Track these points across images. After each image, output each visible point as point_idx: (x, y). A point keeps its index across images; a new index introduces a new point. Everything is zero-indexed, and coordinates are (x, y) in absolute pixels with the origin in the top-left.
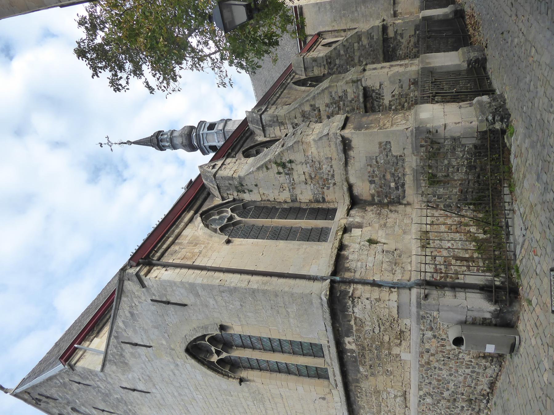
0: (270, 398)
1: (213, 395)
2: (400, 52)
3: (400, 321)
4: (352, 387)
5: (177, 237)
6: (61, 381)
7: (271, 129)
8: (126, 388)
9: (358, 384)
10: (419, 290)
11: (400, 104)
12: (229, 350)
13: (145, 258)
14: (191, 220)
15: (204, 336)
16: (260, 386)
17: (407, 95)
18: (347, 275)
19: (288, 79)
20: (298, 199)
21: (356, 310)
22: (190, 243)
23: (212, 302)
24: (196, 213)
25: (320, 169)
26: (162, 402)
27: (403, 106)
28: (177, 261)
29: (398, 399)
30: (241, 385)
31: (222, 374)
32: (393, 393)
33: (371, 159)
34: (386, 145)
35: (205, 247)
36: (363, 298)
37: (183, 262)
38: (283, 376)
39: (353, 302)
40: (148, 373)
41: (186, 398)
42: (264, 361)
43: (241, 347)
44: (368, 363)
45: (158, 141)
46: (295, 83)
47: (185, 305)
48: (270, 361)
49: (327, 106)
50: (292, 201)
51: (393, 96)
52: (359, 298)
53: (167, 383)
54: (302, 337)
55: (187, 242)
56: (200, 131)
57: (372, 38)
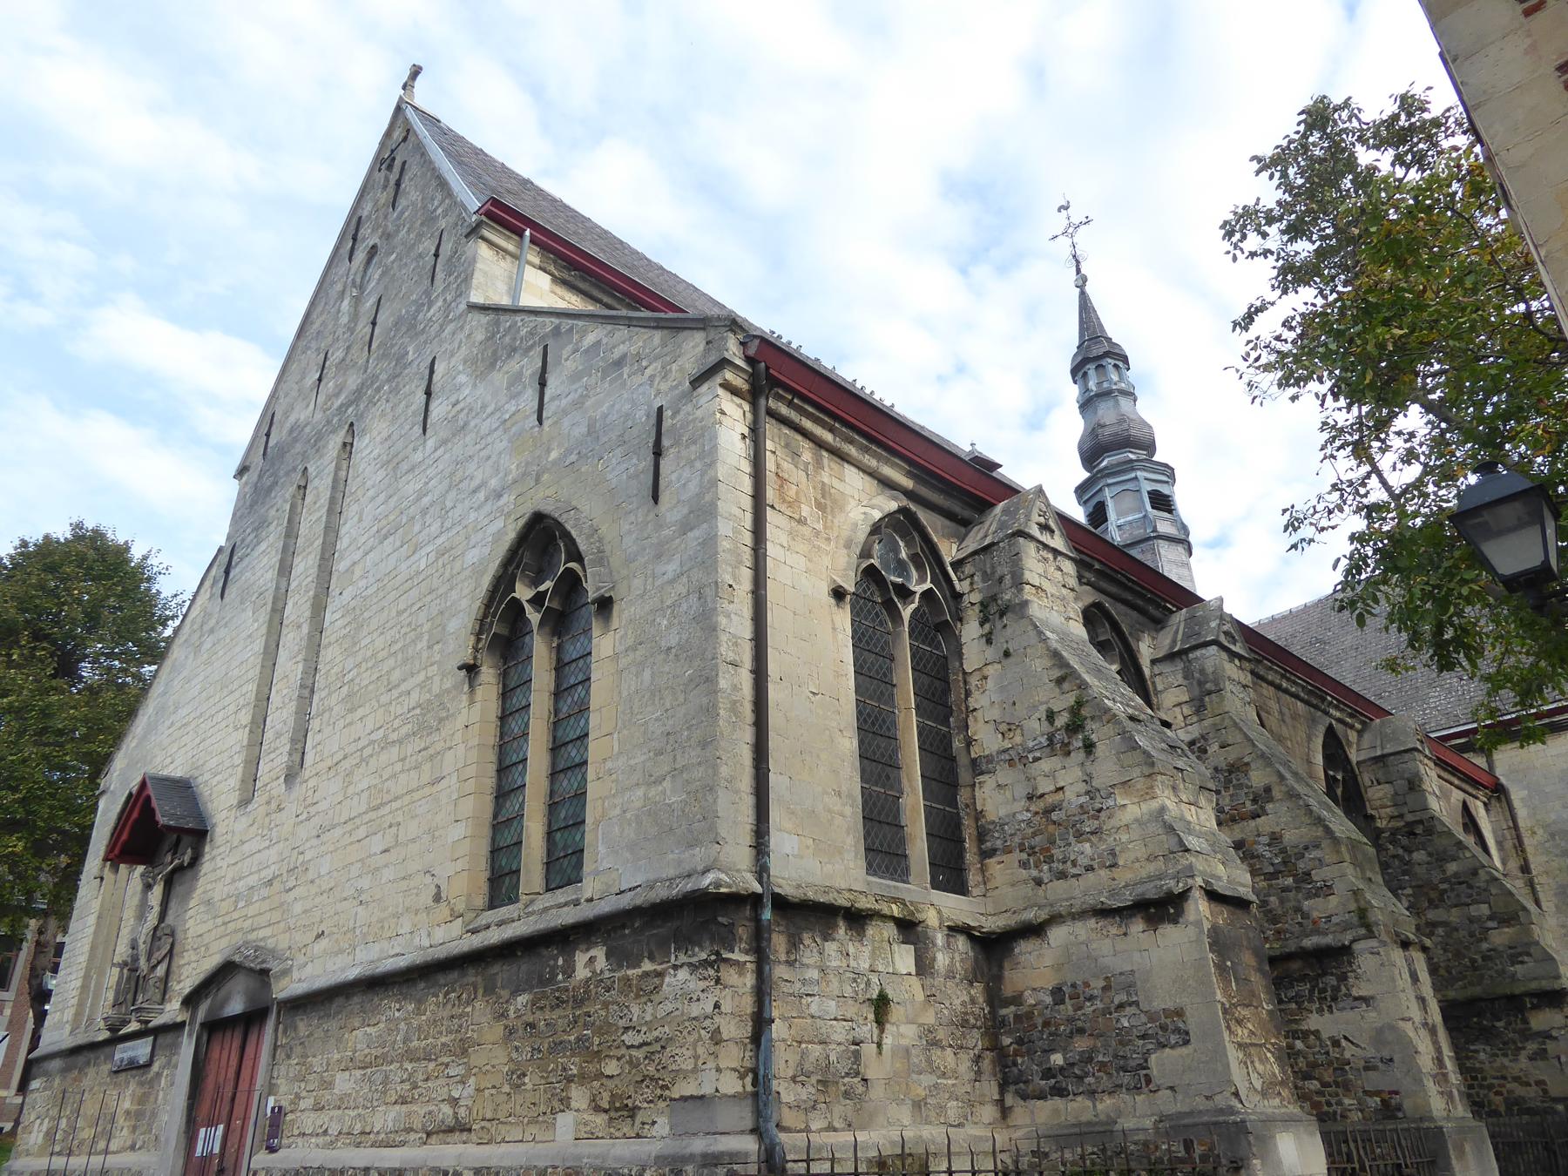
0: (431, 751)
1: (429, 598)
2: (1483, 1055)
3: (662, 1104)
4: (472, 976)
5: (835, 452)
6: (440, 211)
7: (1180, 676)
8: (432, 372)
9: (481, 991)
10: (754, 1158)
11: (1314, 1065)
12: (547, 629)
13: (769, 377)
14: (887, 484)
15: (579, 558)
16: (460, 721)
17: (1347, 1087)
18: (779, 942)
19: (1341, 710)
20: (981, 778)
21: (683, 974)
22: (823, 489)
23: (671, 568)
24: (909, 494)
25: (1079, 835)
26: (405, 466)
27: (1307, 1077)
28: (770, 465)
29: (447, 1109)
30: (460, 668)
31: (485, 616)
32: (464, 1093)
33: (1129, 987)
34: (1177, 1031)
35: (817, 534)
36: (717, 992)
37: (770, 477)
38: (490, 782)
39: (706, 964)
40: (472, 424)
41: (417, 528)
42: (527, 725)
43: (559, 660)
44: (541, 1018)
45: (1097, 357)
46: (1330, 731)
47: (655, 498)
48: (526, 741)
49: (1275, 838)
50: (974, 762)
51: (1336, 1043)
52: (718, 981)
53: (452, 474)
54: (597, 823)
55: (826, 480)
56: (1144, 469)
57: (1515, 959)
